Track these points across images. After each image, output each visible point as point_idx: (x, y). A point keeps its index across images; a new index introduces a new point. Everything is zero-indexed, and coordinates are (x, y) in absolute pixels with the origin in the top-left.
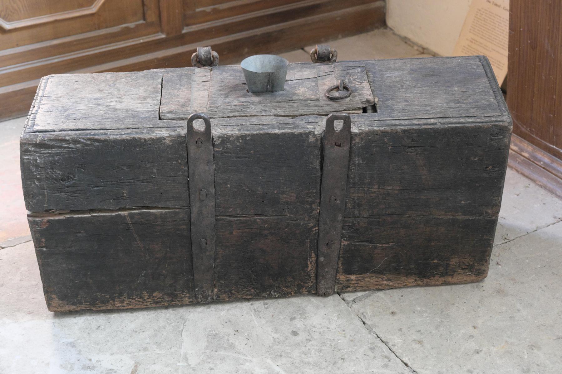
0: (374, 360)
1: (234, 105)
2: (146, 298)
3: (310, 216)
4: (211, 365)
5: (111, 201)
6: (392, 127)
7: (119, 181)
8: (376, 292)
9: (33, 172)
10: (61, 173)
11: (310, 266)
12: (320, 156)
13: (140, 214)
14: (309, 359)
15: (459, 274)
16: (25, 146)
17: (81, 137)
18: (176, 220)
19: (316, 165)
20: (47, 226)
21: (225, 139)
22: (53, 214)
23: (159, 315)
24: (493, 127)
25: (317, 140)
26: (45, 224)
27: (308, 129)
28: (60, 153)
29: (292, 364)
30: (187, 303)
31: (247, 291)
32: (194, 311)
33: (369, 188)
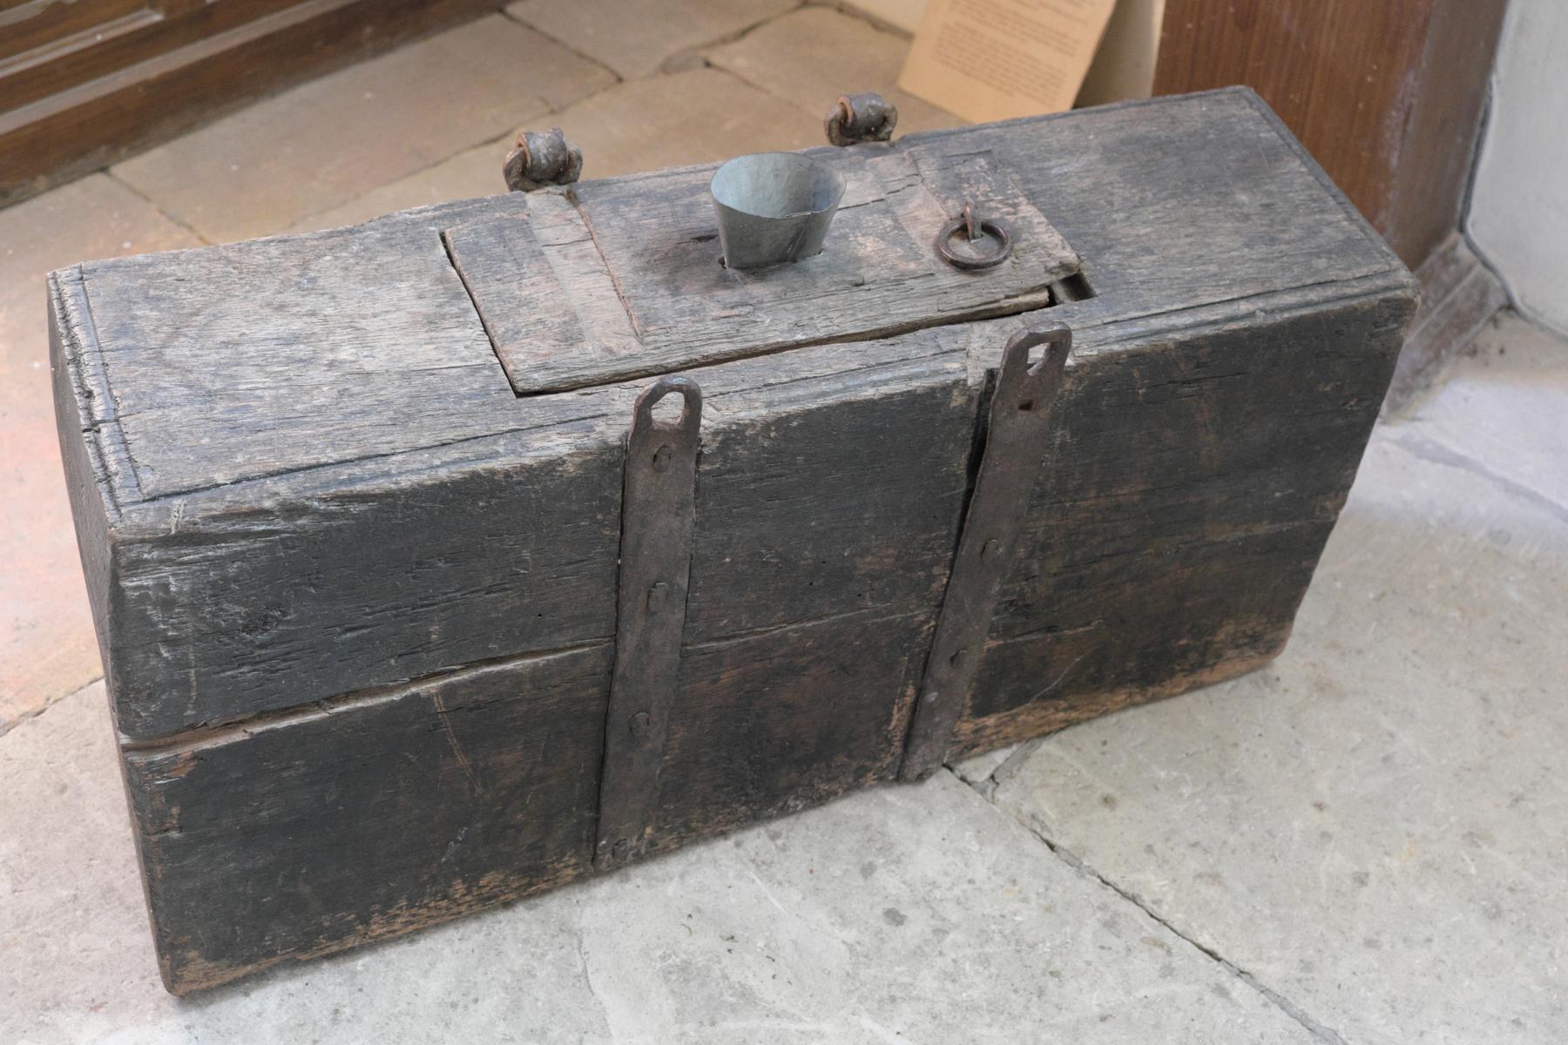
0: (1131, 958)
1: (714, 319)
2: (457, 896)
3: (924, 597)
5: (393, 662)
6: (1152, 338)
7: (419, 603)
8: (1036, 741)
9: (154, 625)
10: (243, 610)
11: (896, 716)
12: (970, 442)
13: (473, 682)
14: (969, 992)
15: (1229, 659)
16: (130, 551)
17: (308, 494)
18: (574, 679)
19: (959, 465)
20: (190, 769)
21: (732, 436)
22: (196, 729)
23: (494, 933)
24: (1382, 304)
25: (970, 399)
26: (184, 766)
27: (949, 373)
28: (243, 552)
29: (935, 1018)
30: (569, 879)
31: (729, 813)
32: (590, 898)
33: (1076, 501)
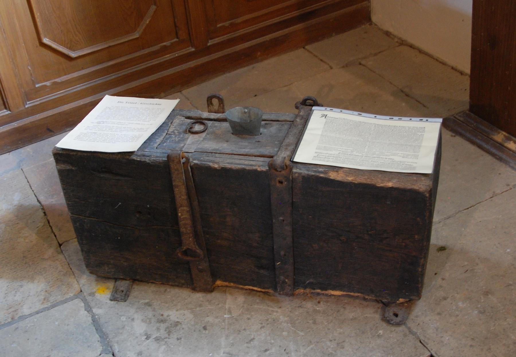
4: (249, 316)
